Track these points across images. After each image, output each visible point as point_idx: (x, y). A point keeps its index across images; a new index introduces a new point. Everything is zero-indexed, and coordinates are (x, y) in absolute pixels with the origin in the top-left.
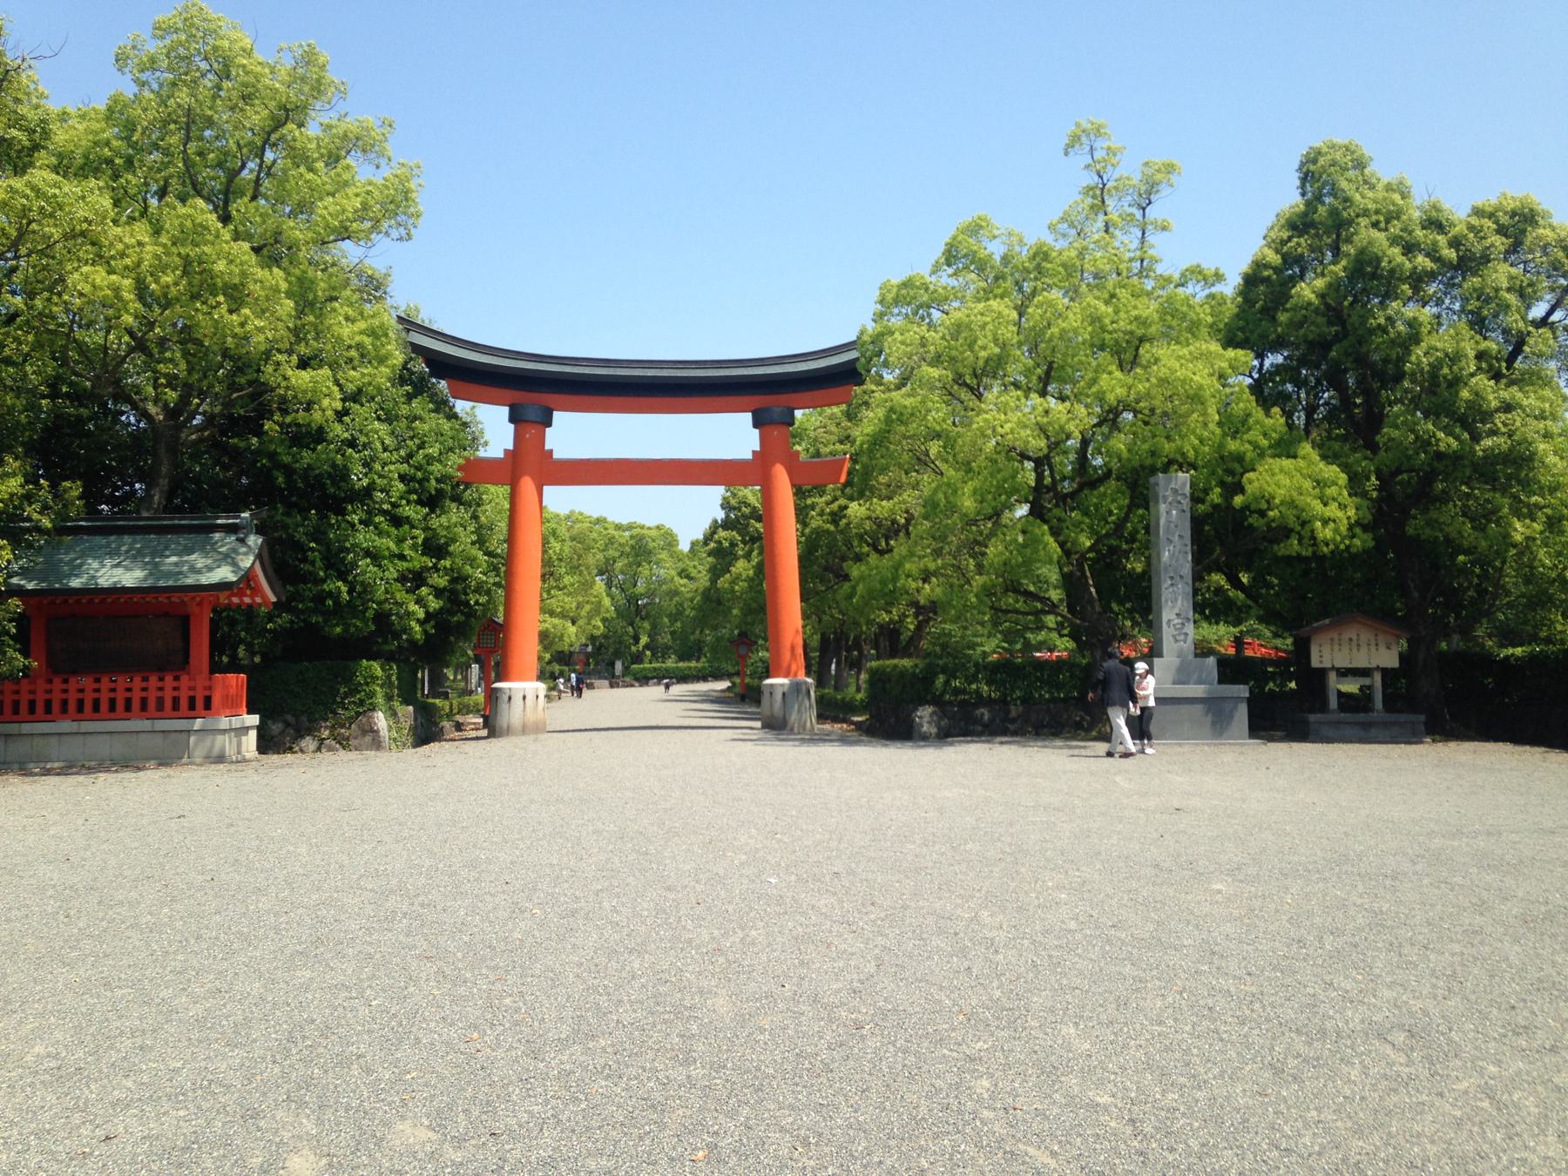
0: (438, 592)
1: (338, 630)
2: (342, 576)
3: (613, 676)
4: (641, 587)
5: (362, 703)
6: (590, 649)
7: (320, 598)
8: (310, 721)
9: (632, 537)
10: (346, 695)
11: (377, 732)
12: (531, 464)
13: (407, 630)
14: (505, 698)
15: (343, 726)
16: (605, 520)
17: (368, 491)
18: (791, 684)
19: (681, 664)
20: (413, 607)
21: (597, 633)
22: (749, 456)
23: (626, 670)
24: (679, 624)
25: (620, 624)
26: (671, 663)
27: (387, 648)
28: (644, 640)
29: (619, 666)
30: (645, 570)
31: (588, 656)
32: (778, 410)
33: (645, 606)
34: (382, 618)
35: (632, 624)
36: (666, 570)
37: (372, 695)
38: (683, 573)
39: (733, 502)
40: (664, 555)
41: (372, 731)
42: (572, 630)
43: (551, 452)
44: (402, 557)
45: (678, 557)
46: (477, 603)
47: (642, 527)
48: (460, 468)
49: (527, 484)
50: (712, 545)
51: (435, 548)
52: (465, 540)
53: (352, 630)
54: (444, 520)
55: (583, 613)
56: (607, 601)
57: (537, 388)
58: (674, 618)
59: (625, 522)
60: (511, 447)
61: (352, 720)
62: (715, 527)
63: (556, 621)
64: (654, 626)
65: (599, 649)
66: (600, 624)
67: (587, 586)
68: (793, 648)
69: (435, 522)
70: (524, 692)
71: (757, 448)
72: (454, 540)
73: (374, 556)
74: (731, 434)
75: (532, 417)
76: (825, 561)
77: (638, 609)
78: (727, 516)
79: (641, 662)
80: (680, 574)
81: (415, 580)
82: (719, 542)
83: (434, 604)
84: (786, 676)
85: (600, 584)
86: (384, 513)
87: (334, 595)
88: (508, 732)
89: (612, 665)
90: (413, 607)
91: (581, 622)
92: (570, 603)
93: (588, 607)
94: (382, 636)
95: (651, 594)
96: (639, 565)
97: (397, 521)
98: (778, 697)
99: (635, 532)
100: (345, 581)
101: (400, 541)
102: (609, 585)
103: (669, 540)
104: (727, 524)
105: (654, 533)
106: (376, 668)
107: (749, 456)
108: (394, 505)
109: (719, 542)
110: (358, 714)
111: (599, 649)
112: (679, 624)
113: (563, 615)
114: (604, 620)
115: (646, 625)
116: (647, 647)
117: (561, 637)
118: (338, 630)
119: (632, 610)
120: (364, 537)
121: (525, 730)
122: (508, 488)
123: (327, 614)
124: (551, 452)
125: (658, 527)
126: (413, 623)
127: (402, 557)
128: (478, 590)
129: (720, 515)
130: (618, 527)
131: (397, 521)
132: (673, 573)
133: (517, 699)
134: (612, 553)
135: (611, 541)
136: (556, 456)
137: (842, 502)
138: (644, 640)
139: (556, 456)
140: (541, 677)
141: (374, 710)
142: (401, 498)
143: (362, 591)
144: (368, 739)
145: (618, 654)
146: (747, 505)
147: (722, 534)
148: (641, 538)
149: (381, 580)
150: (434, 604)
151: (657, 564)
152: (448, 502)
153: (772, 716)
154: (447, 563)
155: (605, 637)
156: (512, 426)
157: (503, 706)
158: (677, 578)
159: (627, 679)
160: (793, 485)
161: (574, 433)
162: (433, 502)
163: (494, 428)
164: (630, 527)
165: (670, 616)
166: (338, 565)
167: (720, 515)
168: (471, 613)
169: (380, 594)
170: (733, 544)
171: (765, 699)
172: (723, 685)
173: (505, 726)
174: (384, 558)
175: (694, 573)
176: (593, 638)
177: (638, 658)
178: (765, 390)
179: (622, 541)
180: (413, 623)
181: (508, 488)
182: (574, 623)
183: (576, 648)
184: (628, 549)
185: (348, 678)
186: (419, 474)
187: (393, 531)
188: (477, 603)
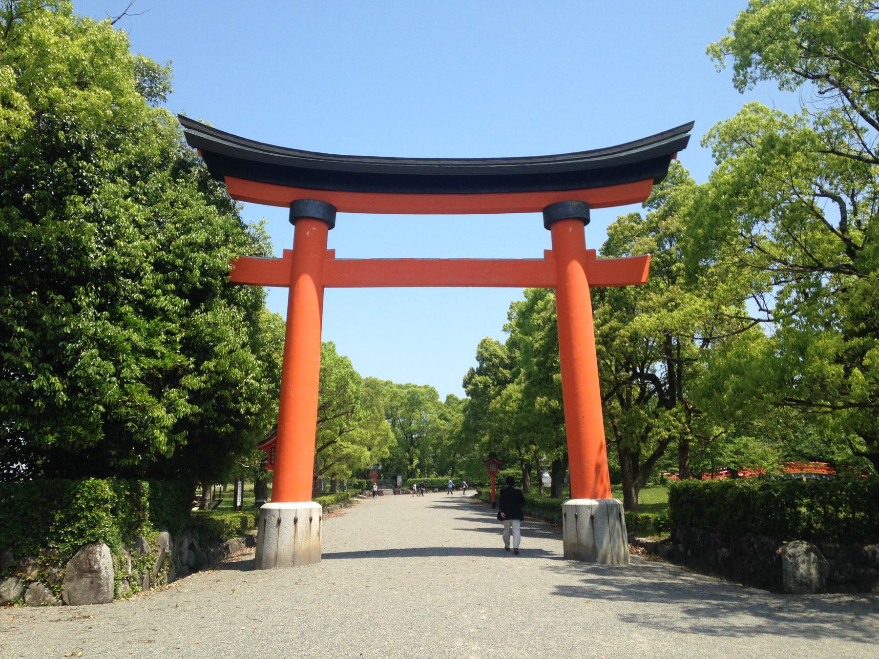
0: (195, 397)
1: (51, 439)
2: (60, 371)
3: (396, 486)
4: (414, 426)
5: (81, 533)
6: (380, 467)
7: (26, 398)
8: (16, 557)
9: (408, 393)
10: (63, 523)
11: (98, 571)
12: (313, 266)
13: (150, 442)
14: (274, 521)
15: (55, 565)
16: (391, 382)
17: (109, 273)
18: (601, 507)
19: (440, 478)
20: (160, 412)
21: (385, 456)
22: (541, 256)
23: (404, 482)
24: (439, 451)
25: (400, 452)
26: (433, 477)
27: (125, 462)
28: (416, 461)
29: (400, 479)
30: (417, 415)
31: (379, 472)
32: (575, 204)
33: (417, 438)
34: (114, 424)
35: (408, 451)
36: (430, 415)
37: (94, 523)
38: (442, 417)
39: (486, 354)
40: (429, 405)
41: (91, 571)
42: (368, 453)
43: (333, 251)
44: (151, 353)
45: (439, 406)
46: (248, 412)
47: (415, 386)
48: (232, 261)
49: (307, 283)
50: (470, 387)
51: (198, 348)
52: (235, 338)
53: (71, 439)
54: (210, 317)
55: (376, 442)
56: (392, 435)
57: (319, 183)
58: (436, 447)
59: (404, 383)
60: (290, 247)
61: (65, 558)
62: (472, 373)
63: (355, 447)
64: (423, 452)
65: (387, 467)
66: (387, 450)
67: (377, 422)
68: (598, 468)
69: (199, 317)
70: (297, 515)
71: (550, 247)
72: (220, 340)
73: (109, 350)
74: (522, 234)
75: (312, 213)
76: (623, 367)
77: (412, 442)
78: (481, 366)
79: (414, 477)
80: (440, 417)
81: (160, 382)
82: (476, 385)
83: (185, 408)
84: (594, 496)
85: (387, 424)
86: (131, 302)
87: (50, 397)
88: (276, 562)
89: (395, 478)
90: (160, 412)
91: (375, 449)
92: (366, 434)
93: (379, 438)
94: (116, 448)
95: (420, 431)
96: (413, 411)
97: (149, 312)
98: (585, 521)
99: (410, 389)
100: (62, 376)
101: (152, 334)
102: (393, 425)
103: (432, 394)
104: (480, 372)
105: (423, 390)
106: (105, 488)
107: (541, 256)
108: (147, 294)
109: (476, 385)
110: (76, 548)
111: (386, 468)
112: (439, 451)
113: (361, 443)
114: (390, 448)
115: (418, 451)
116: (418, 466)
117: (359, 459)
118: (51, 439)
119: (409, 442)
120: (88, 322)
121: (295, 560)
122: (286, 290)
123: (38, 419)
124: (333, 251)
125: (425, 387)
126: (157, 432)
127: (151, 353)
128: (251, 399)
129: (476, 365)
130: (399, 387)
131: (149, 312)
132: (436, 416)
133: (287, 523)
134: (396, 403)
135: (395, 395)
136: (338, 256)
137: (614, 323)
138: (416, 461)
139: (338, 256)
140: (316, 494)
141: (96, 542)
142: (157, 287)
143: (84, 389)
144: (86, 581)
145: (399, 471)
146: (496, 356)
147: (478, 378)
148: (415, 393)
149: (120, 385)
150: (185, 408)
151: (425, 410)
152: (217, 299)
153: (579, 544)
154: (210, 364)
155: (391, 459)
156: (292, 228)
157: (272, 530)
158: (438, 420)
159: (405, 488)
160: (590, 286)
161: (356, 234)
162: (200, 297)
163: (271, 225)
164: (407, 386)
165: (433, 445)
166: (54, 353)
167: (476, 365)
168: (241, 424)
169: (113, 391)
170: (486, 386)
171: (569, 525)
172: (471, 493)
173: (273, 555)
174: (124, 351)
175: (449, 416)
176: (383, 460)
177: (412, 474)
178: (558, 185)
179: (402, 395)
180: (157, 432)
181: (286, 290)
182: (370, 449)
183: (371, 467)
184: (406, 401)
185: (66, 503)
186: (179, 262)
187: (142, 322)
188: (248, 412)
